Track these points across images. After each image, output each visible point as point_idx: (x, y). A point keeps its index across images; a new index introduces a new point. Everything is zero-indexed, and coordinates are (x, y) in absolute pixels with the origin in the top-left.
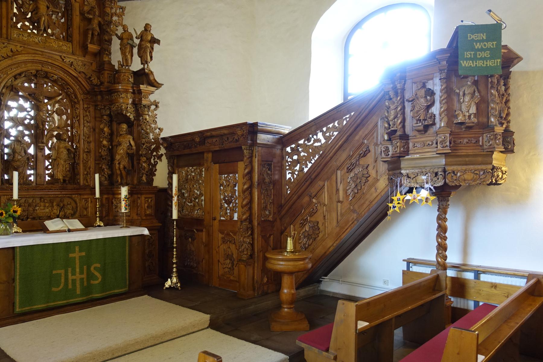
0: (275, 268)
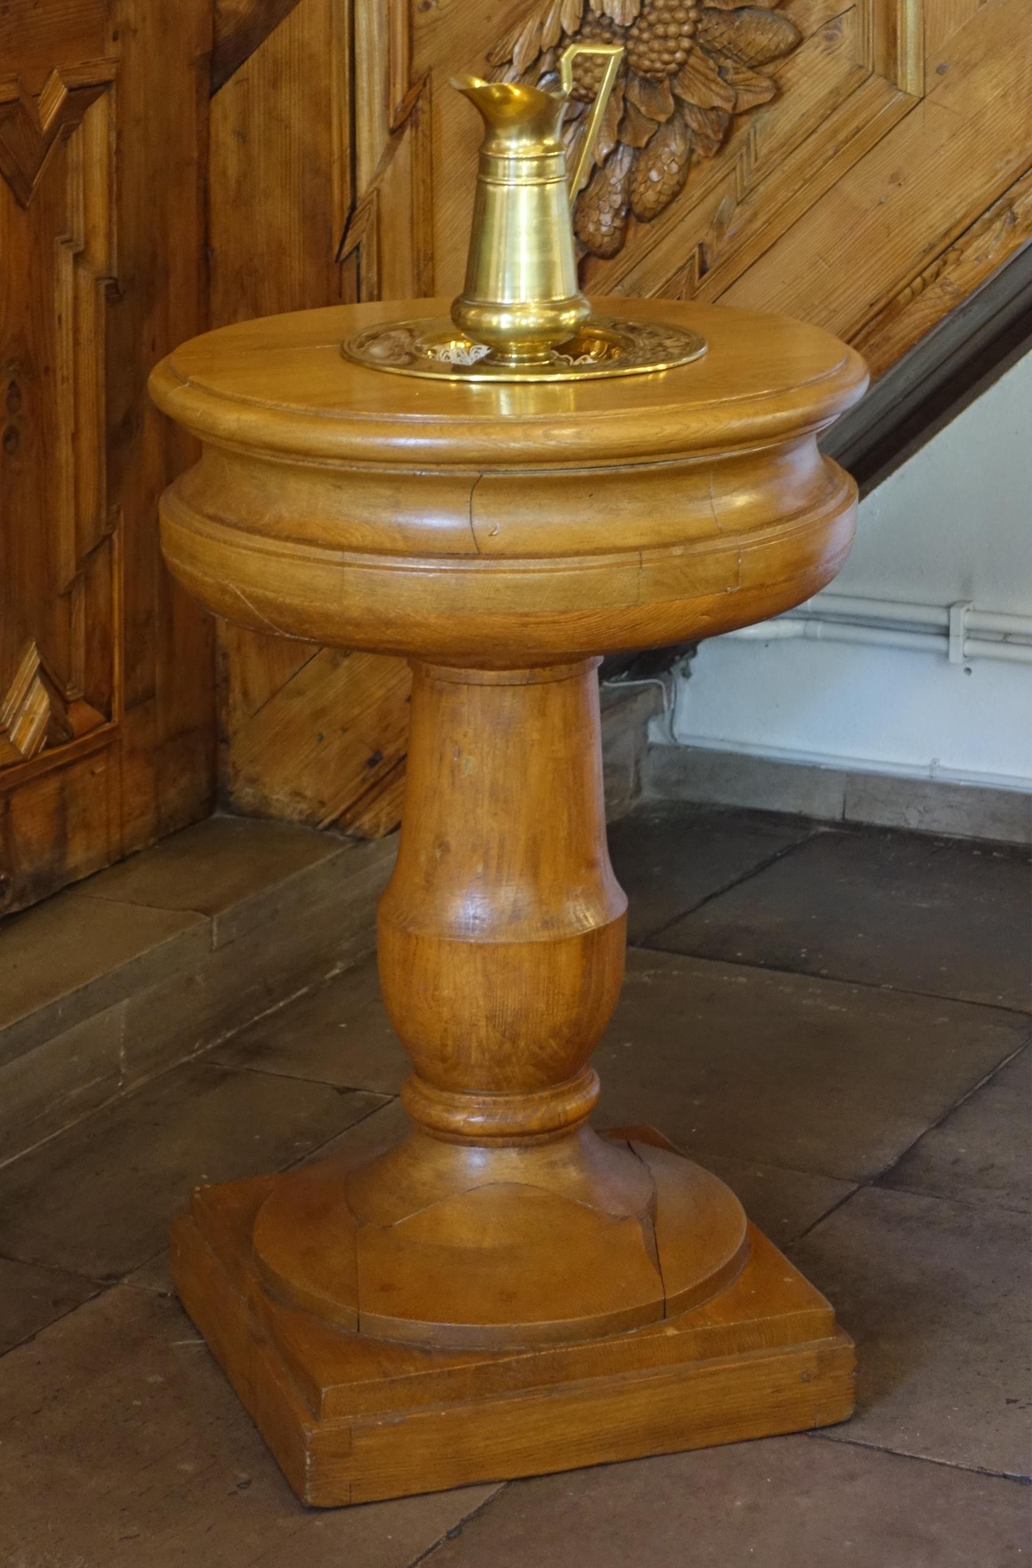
0: (356, 604)
